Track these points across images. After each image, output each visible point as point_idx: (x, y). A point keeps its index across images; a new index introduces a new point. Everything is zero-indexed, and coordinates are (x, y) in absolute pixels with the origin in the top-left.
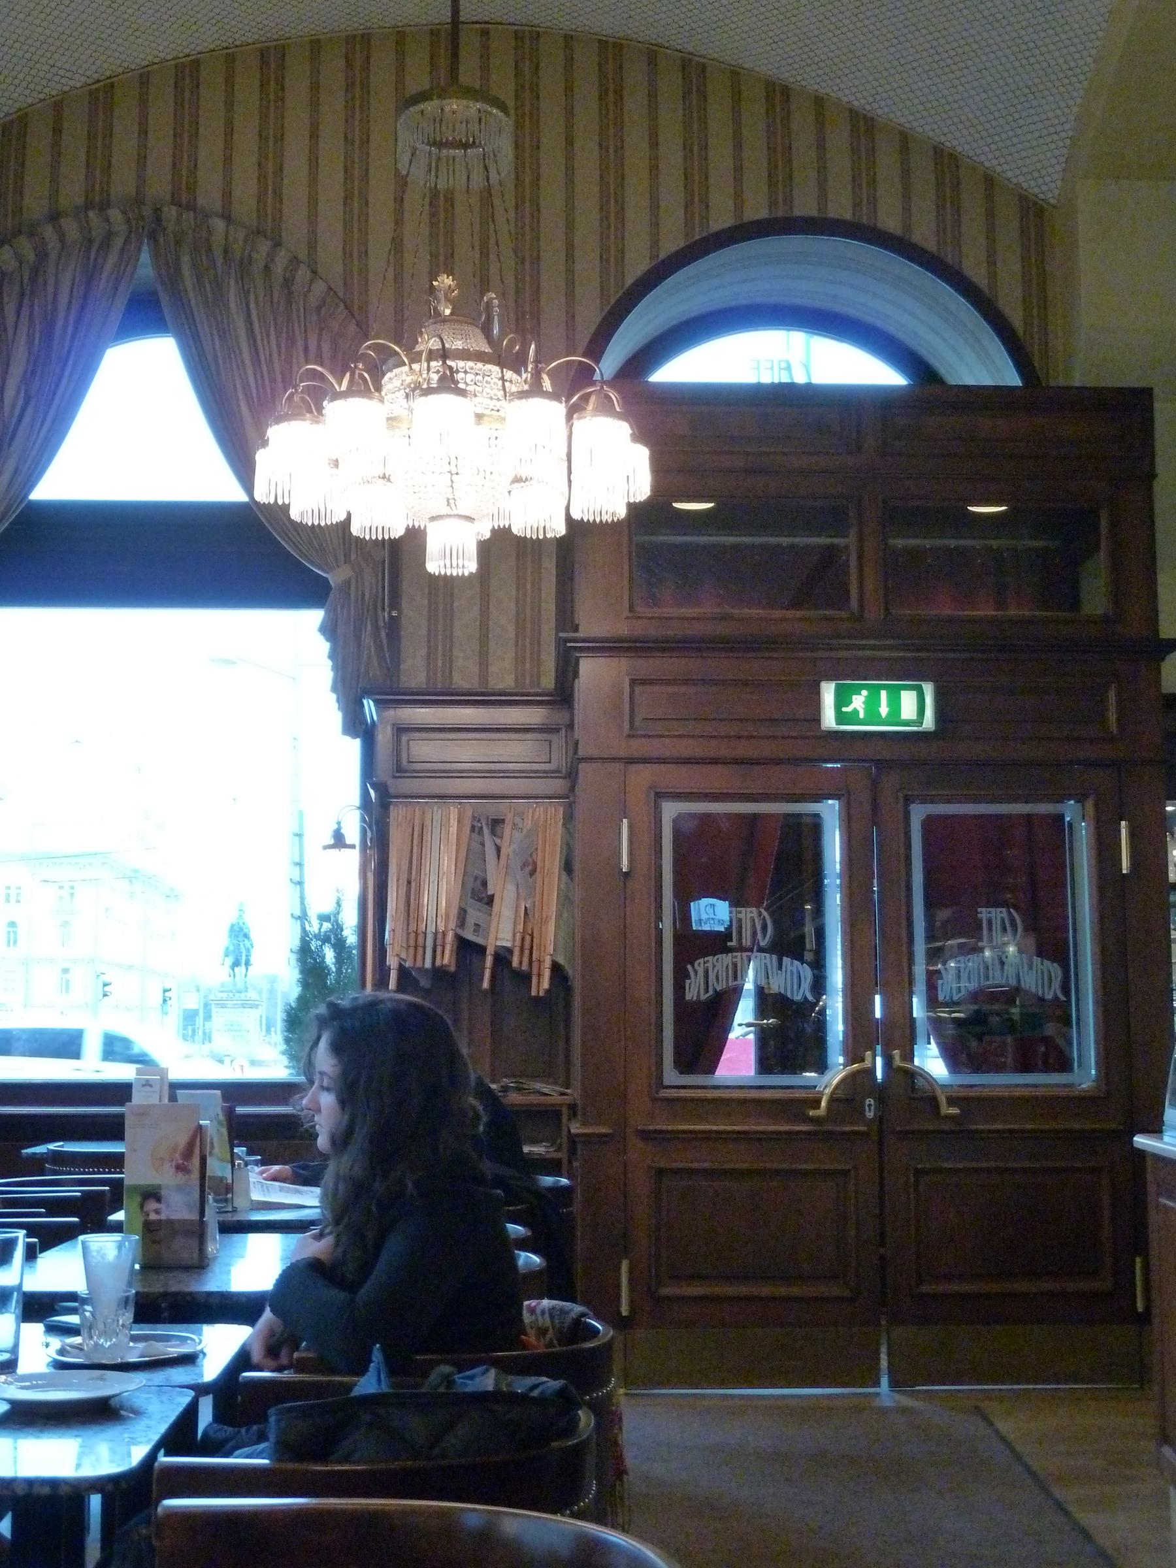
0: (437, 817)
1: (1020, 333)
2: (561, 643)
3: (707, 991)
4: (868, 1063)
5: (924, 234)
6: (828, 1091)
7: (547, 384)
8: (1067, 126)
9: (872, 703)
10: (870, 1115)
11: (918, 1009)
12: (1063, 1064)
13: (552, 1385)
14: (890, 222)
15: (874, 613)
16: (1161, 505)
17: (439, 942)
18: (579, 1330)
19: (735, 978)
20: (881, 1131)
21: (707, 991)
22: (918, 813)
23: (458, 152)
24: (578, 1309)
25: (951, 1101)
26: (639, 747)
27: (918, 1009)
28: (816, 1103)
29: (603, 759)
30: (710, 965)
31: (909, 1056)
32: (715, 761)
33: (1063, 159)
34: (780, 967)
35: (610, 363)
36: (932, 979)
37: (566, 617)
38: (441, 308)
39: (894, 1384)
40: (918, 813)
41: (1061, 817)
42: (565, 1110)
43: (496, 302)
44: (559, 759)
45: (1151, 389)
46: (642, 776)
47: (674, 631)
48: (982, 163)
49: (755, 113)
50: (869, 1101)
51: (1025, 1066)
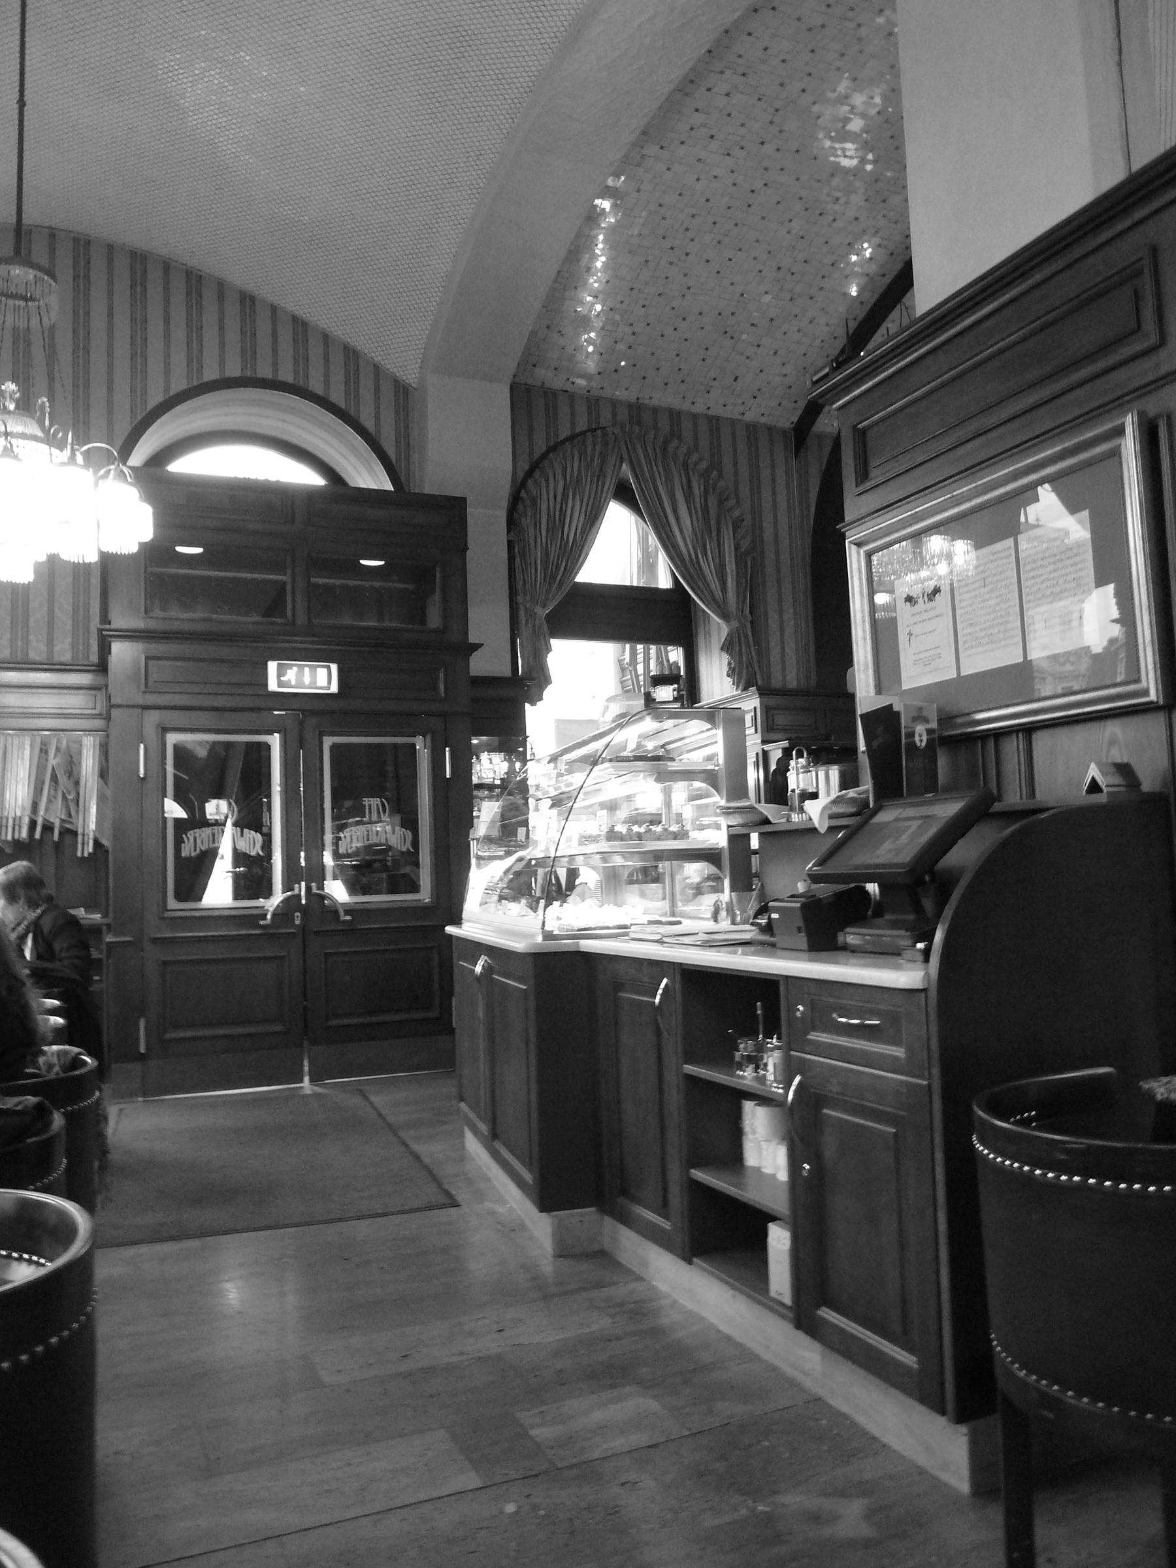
0: (16, 742)
1: (394, 461)
2: (100, 631)
3: (195, 850)
4: (296, 891)
5: (337, 396)
6: (271, 909)
7: (80, 459)
8: (422, 341)
9: (300, 675)
10: (297, 922)
11: (328, 859)
12: (414, 888)
13: (32, 1100)
14: (316, 387)
15: (301, 619)
16: (471, 567)
17: (17, 822)
18: (76, 1063)
19: (214, 842)
20: (304, 930)
21: (195, 850)
22: (328, 742)
23: (22, 303)
24: (76, 1050)
25: (347, 912)
26: (151, 699)
27: (328, 859)
28: (264, 916)
29: (128, 706)
30: (197, 835)
31: (321, 887)
32: (201, 709)
33: (419, 361)
34: (242, 835)
35: (138, 458)
36: (337, 841)
37: (105, 619)
38: (7, 404)
39: (311, 1081)
40: (328, 742)
41: (414, 745)
42: (104, 927)
43: (47, 404)
44: (101, 707)
45: (465, 499)
46: (153, 717)
47: (176, 626)
48: (372, 358)
49: (233, 310)
50: (298, 914)
51: (392, 891)
